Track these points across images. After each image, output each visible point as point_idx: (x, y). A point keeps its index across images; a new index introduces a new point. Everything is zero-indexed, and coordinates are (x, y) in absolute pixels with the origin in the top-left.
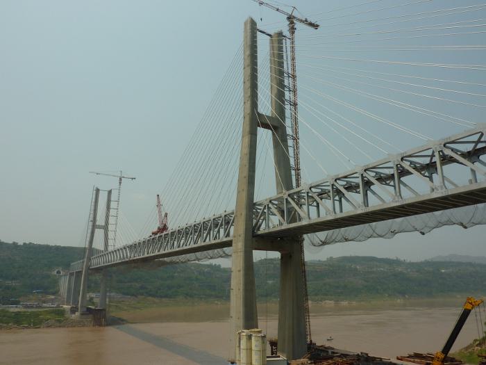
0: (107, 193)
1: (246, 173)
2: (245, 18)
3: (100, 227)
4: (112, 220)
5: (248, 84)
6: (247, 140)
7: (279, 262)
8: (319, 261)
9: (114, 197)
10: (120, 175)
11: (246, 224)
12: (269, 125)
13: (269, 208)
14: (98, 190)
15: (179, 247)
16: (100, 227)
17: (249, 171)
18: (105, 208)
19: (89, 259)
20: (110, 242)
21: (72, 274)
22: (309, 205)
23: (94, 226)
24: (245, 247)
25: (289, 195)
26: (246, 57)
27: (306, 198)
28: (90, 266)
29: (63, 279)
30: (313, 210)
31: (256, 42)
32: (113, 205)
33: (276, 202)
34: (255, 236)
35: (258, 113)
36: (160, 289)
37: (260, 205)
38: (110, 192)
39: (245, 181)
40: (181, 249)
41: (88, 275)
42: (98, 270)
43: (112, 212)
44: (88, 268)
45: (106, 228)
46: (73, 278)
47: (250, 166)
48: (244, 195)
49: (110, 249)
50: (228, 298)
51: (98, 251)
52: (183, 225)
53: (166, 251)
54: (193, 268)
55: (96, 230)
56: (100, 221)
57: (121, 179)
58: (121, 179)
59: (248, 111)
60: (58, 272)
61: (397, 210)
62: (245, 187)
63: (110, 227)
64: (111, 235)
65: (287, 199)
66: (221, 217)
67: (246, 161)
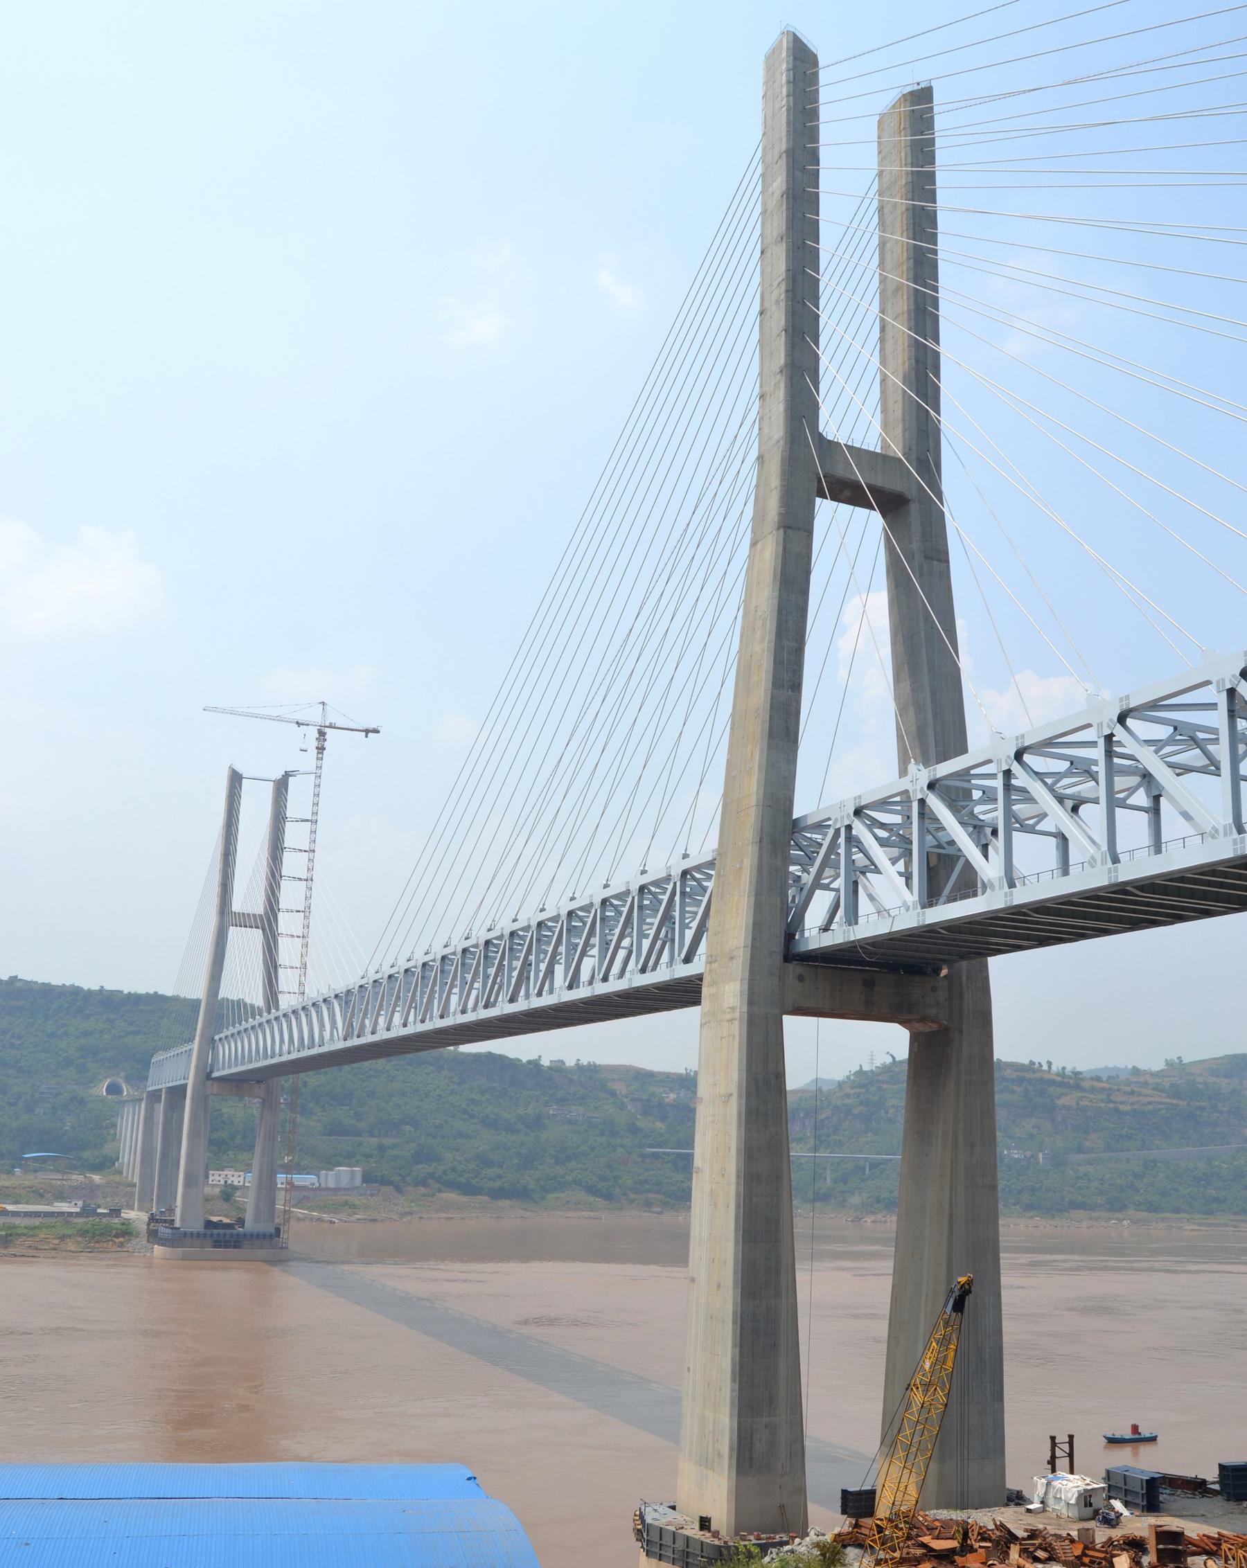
0: (269, 789)
1: (760, 695)
2: (768, 37)
3: (245, 921)
4: (290, 895)
5: (779, 318)
6: (770, 550)
7: (905, 1067)
8: (1136, 1071)
9: (297, 803)
10: (317, 719)
11: (758, 908)
12: (856, 486)
13: (851, 840)
14: (236, 779)
15: (464, 1012)
16: (245, 921)
17: (777, 683)
18: (265, 855)
19: (210, 1043)
20: (287, 980)
21: (154, 1096)
22: (1114, 803)
23: (226, 916)
24: (751, 1002)
25: (931, 786)
26: (772, 204)
27: (1100, 769)
28: (211, 1072)
29: (128, 1110)
30: (1132, 826)
31: (813, 135)
32: (294, 835)
33: (898, 799)
34: (791, 953)
35: (820, 439)
36: (488, 1163)
37: (820, 826)
38: (281, 787)
39: (757, 727)
40: (582, 993)
41: (201, 1101)
42: (240, 1083)
43: (292, 864)
44: (206, 1076)
45: (268, 923)
46: (160, 1108)
47: (778, 662)
48: (752, 787)
49: (286, 1002)
50: (682, 1197)
51: (240, 1009)
52: (559, 905)
53: (521, 1006)
54: (620, 1088)
55: (233, 932)
56: (248, 898)
57: (322, 734)
58: (322, 734)
59: (778, 430)
60: (114, 1089)
61: (1226, 875)
62: (755, 754)
63: (287, 923)
64: (287, 951)
65: (922, 802)
66: (668, 878)
67: (763, 649)
